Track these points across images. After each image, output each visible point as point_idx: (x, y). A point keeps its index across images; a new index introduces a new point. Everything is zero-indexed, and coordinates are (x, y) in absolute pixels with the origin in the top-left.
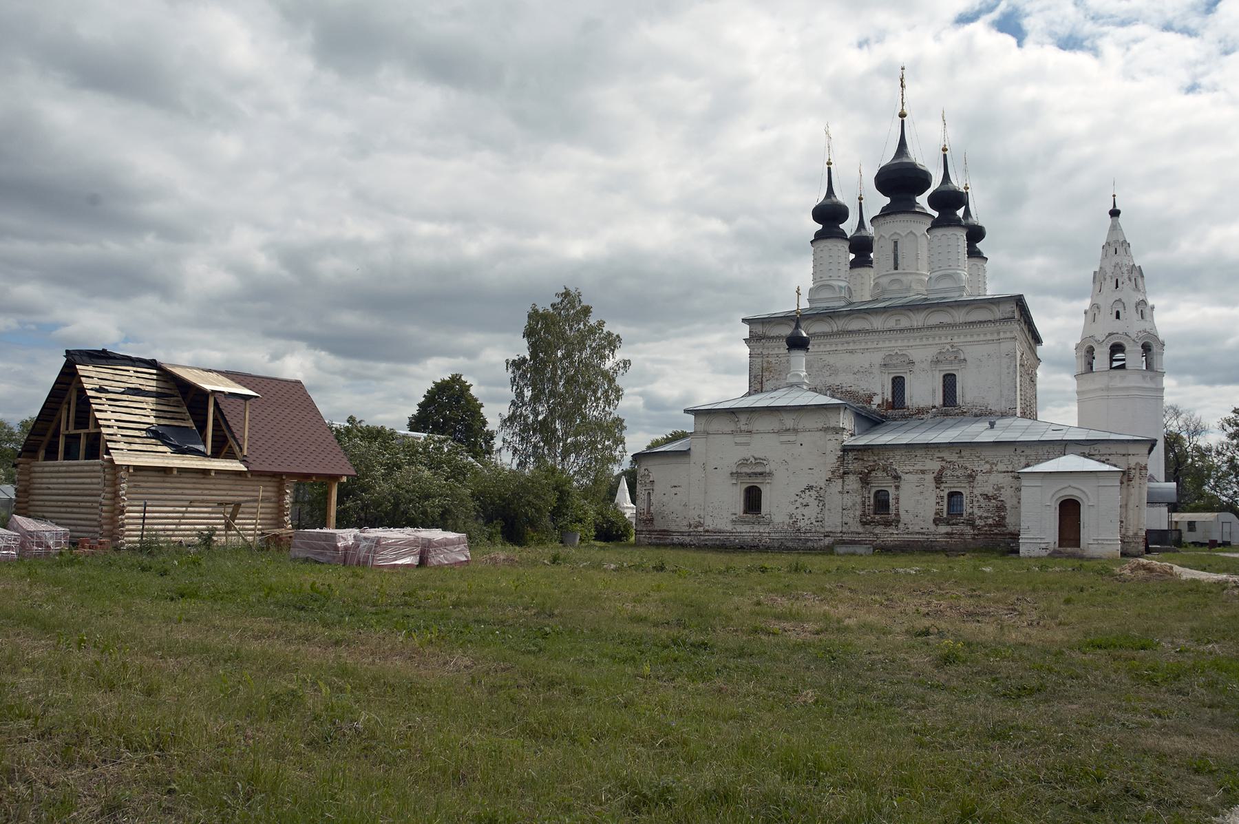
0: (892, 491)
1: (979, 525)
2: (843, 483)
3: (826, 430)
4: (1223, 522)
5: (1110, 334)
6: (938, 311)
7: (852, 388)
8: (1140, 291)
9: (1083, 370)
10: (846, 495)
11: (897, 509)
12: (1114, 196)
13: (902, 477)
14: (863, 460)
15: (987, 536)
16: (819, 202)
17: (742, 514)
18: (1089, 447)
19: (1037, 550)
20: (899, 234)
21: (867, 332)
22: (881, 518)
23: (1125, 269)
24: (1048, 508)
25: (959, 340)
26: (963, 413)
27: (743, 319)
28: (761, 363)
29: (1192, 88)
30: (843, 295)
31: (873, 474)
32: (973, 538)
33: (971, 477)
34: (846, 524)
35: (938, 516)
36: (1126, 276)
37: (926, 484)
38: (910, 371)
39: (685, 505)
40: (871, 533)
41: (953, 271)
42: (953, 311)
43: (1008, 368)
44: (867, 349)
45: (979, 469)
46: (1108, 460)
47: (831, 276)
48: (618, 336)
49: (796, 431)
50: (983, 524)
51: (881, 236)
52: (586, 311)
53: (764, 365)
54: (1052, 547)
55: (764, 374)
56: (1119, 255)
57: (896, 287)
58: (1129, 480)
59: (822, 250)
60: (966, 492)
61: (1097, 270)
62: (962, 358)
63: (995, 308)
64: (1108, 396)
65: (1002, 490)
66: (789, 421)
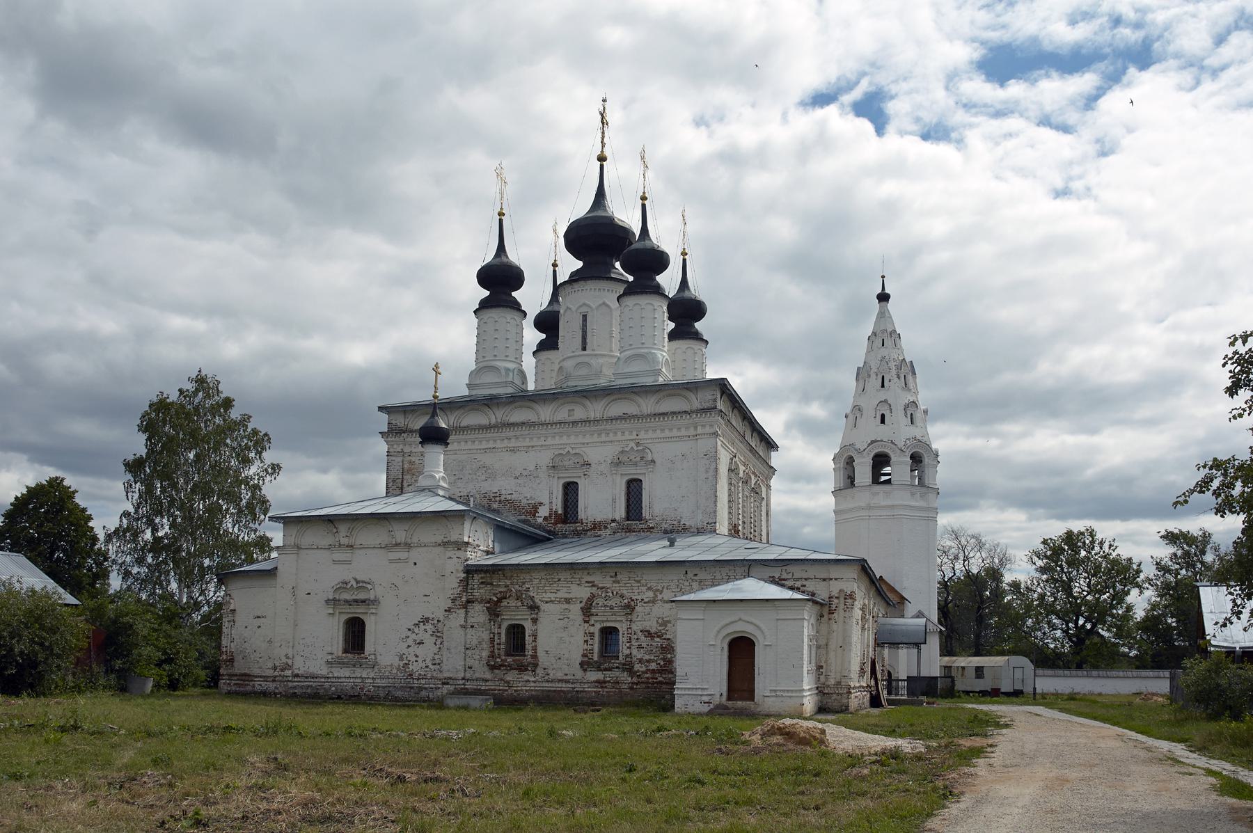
0: (528, 626)
1: (638, 671)
2: (467, 614)
3: (445, 544)
4: (1014, 668)
5: (873, 442)
6: (621, 399)
7: (513, 496)
8: (909, 390)
10: (469, 630)
11: (535, 649)
12: (883, 277)
13: (542, 608)
14: (492, 584)
15: (650, 685)
16: (486, 262)
17: (340, 654)
18: (780, 569)
19: (698, 704)
20: (588, 306)
21: (531, 424)
22: (513, 660)
23: (892, 364)
24: (712, 649)
25: (646, 437)
26: (650, 529)
27: (379, 407)
28: (401, 464)
29: (1062, 193)
30: (510, 379)
31: (504, 603)
32: (631, 688)
33: (629, 608)
34: (470, 668)
35: (586, 659)
36: (894, 372)
37: (571, 617)
38: (585, 475)
39: (270, 642)
40: (501, 680)
41: (646, 351)
42: (638, 398)
43: (707, 472)
44: (533, 447)
45: (639, 598)
46: (805, 586)
47: (495, 356)
48: (266, 435)
49: (408, 546)
50: (644, 669)
51: (568, 308)
52: (228, 403)
53: (405, 466)
54: (717, 700)
55: (405, 477)
56: (886, 348)
57: (583, 371)
58: (831, 612)
59: (486, 323)
60: (622, 628)
61: (861, 365)
62: (650, 459)
63: (692, 396)
65: (669, 625)
66: (400, 533)
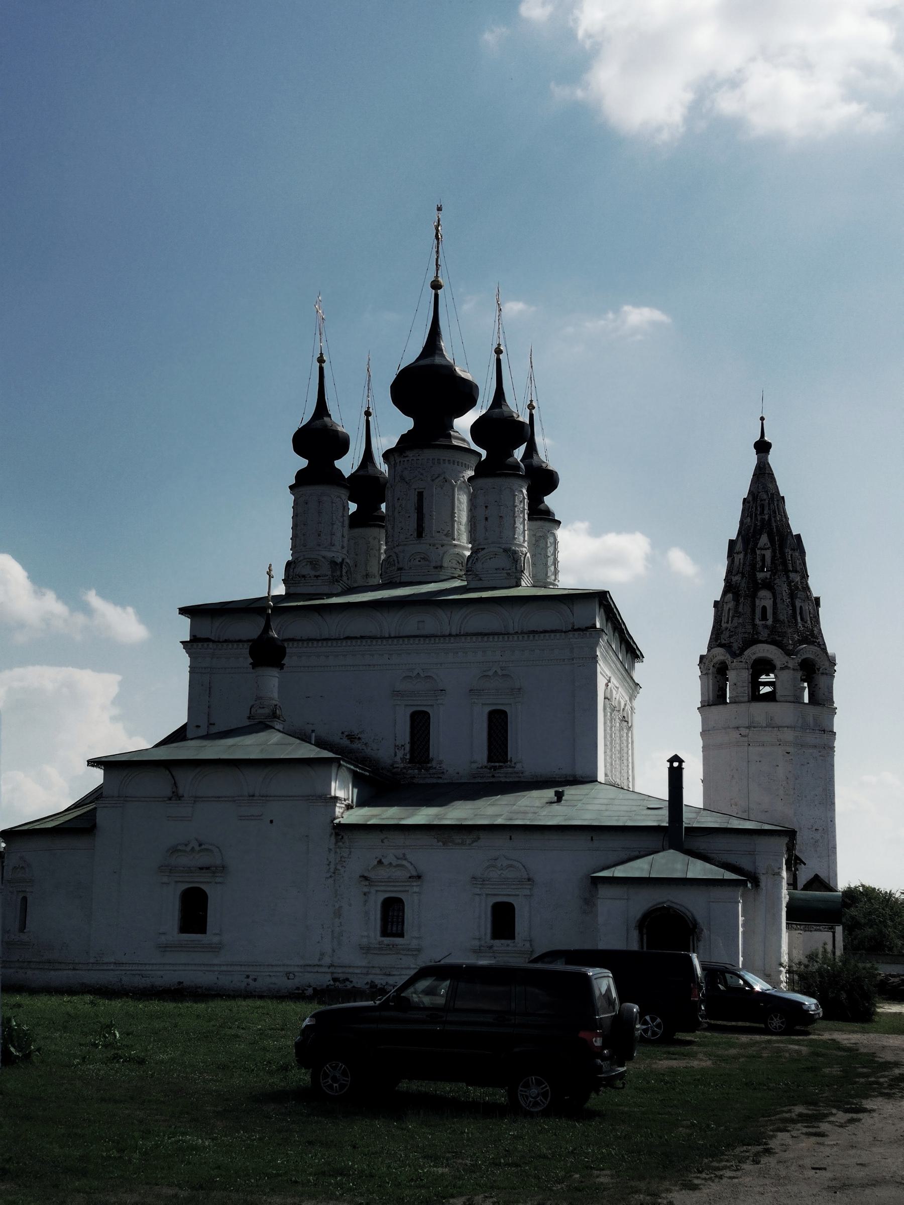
9: (711, 699)
64: (74, 969)
66: (253, 781)
